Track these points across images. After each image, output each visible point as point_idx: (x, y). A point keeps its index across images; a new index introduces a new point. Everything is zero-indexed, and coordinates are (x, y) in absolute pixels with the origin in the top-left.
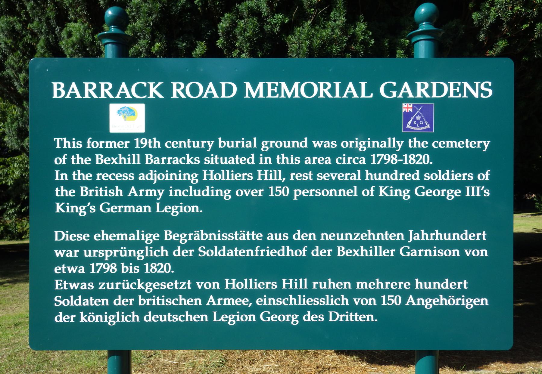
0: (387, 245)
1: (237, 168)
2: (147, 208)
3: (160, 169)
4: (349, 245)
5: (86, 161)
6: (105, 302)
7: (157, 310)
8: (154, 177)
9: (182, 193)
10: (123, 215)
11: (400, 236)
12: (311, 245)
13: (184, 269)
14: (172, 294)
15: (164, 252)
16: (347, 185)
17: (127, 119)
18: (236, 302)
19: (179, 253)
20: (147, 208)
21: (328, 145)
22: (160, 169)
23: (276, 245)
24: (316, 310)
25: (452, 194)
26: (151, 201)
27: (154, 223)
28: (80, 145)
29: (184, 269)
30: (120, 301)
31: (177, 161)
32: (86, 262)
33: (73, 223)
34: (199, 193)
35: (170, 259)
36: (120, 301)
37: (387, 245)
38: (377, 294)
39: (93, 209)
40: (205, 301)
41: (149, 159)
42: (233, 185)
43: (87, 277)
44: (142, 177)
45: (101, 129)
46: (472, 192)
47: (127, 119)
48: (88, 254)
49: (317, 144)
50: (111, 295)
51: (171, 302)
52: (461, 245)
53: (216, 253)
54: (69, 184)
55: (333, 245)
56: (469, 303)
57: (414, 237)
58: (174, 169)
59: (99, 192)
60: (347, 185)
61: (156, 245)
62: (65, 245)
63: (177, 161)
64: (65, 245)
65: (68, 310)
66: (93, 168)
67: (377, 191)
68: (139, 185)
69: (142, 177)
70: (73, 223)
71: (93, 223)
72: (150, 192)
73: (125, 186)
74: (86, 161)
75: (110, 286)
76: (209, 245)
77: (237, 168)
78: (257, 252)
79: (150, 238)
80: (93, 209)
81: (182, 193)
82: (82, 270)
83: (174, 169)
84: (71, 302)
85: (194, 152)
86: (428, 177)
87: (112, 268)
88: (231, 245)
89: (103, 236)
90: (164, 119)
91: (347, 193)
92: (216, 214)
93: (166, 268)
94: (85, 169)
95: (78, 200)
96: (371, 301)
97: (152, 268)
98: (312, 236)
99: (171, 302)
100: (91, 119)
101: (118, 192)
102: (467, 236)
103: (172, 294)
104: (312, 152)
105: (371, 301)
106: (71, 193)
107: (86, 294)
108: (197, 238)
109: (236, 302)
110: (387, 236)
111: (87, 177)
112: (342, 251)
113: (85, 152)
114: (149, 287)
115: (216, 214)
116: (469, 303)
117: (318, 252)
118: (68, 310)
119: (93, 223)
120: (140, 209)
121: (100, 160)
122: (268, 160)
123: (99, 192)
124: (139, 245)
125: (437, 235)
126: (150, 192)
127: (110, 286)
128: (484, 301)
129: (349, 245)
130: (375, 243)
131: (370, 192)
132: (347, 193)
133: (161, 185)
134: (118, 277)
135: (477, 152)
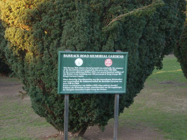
0: (109, 81)
1: (89, 71)
2: (76, 76)
3: (79, 71)
4: (104, 81)
5: (68, 70)
6: (70, 88)
7: (77, 89)
8: (78, 72)
9: (81, 74)
10: (73, 77)
11: (111, 79)
12: (99, 81)
13: (80, 84)
14: (80, 87)
15: (79, 81)
16: (103, 73)
17: (79, 62)
18: (88, 88)
19: (81, 82)
20: (76, 76)
21: (101, 68)
22: (79, 71)
23: (94, 81)
24: (99, 89)
25: (117, 74)
26: (77, 75)
27: (77, 78)
28: (67, 68)
29: (80, 84)
30: (72, 88)
31: (81, 70)
32: (67, 83)
33: (66, 78)
34: (83, 74)
35: (79, 82)
36: (72, 88)
37: (109, 81)
38: (107, 87)
39: (69, 76)
40: (84, 87)
41: (77, 70)
42: (88, 73)
43: (68, 85)
44: (76, 72)
45: (74, 65)
46: (119, 74)
47: (79, 62)
48: (68, 82)
49: (100, 68)
50: (71, 87)
51: (79, 88)
52: (119, 81)
53: (86, 82)
54: (65, 73)
55: (101, 81)
56: (119, 88)
57: (113, 79)
58: (81, 71)
59: (69, 74)
60: (103, 73)
61: (77, 81)
62: (65, 81)
63: (81, 70)
64: (65, 81)
65: (65, 89)
66: (69, 71)
67: (107, 74)
68: (75, 73)
69: (76, 72)
70: (66, 78)
71: (68, 78)
72: (76, 74)
73: (73, 73)
74: (68, 70)
75: (71, 86)
76: (85, 81)
77: (89, 71)
78: (91, 82)
79: (76, 80)
80: (69, 76)
81: (81, 74)
82: (67, 84)
83: (81, 71)
84: (65, 88)
85: (84, 69)
86: (115, 72)
87: (71, 84)
88: (88, 81)
89: (70, 79)
90: (87, 63)
91: (103, 74)
92: (86, 77)
93: (79, 84)
94: (68, 71)
95: (66, 75)
96: (107, 88)
97: (76, 84)
98: (99, 79)
99: (79, 88)
100: (71, 63)
101: (72, 74)
102: (120, 79)
103: (80, 87)
104: (99, 69)
105: (107, 88)
106: (65, 74)
107: (67, 87)
108: (83, 80)
109: (88, 88)
110: (109, 79)
111: (68, 72)
112: (103, 81)
113: (68, 69)
114: (76, 86)
115: (86, 77)
116: (119, 88)
117: (100, 82)
118: (65, 89)
119: (68, 78)
120: (75, 76)
121: (70, 70)
122: (94, 70)
123: (69, 74)
124: (75, 81)
125: (116, 79)
126: (76, 74)
127: (71, 86)
128: (121, 87)
129: (104, 81)
130: (107, 80)
131: (106, 74)
132: (103, 74)
133: (79, 73)
134: (72, 85)
135: (122, 69)
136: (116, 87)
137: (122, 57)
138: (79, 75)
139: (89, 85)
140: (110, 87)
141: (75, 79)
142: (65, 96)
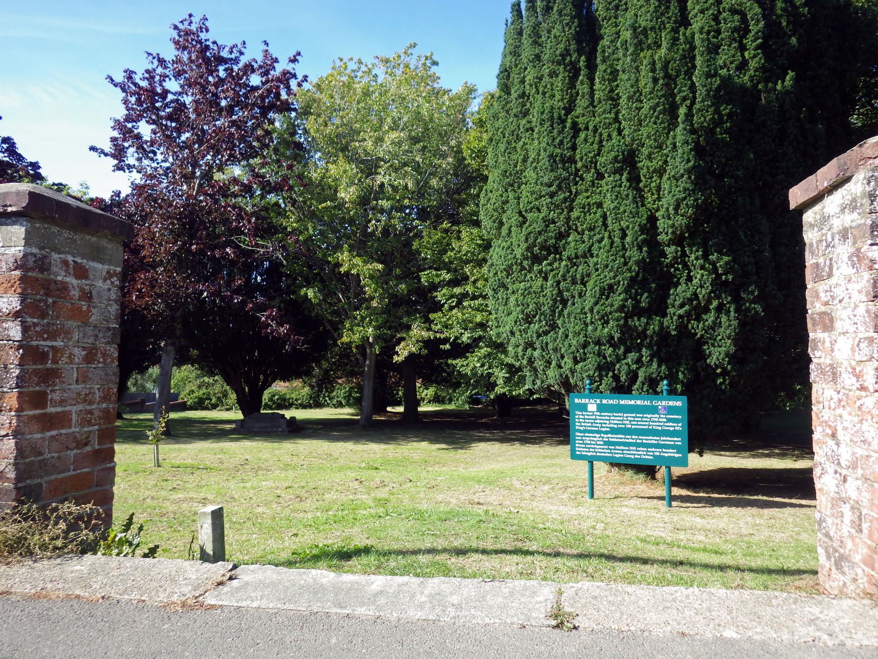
17: (592, 407)
25: (672, 429)
46: (677, 428)
47: (592, 407)
56: (677, 455)
71: (584, 431)
79: (598, 435)
90: (601, 408)
92: (613, 431)
95: (581, 426)
100: (584, 407)
115: (613, 431)
116: (677, 455)
119: (584, 431)
125: (668, 438)
130: (652, 440)
136: (672, 455)
137: (679, 404)
138: (602, 427)
139: (603, 429)
140: (658, 454)
141: (595, 435)
142: (568, 447)
